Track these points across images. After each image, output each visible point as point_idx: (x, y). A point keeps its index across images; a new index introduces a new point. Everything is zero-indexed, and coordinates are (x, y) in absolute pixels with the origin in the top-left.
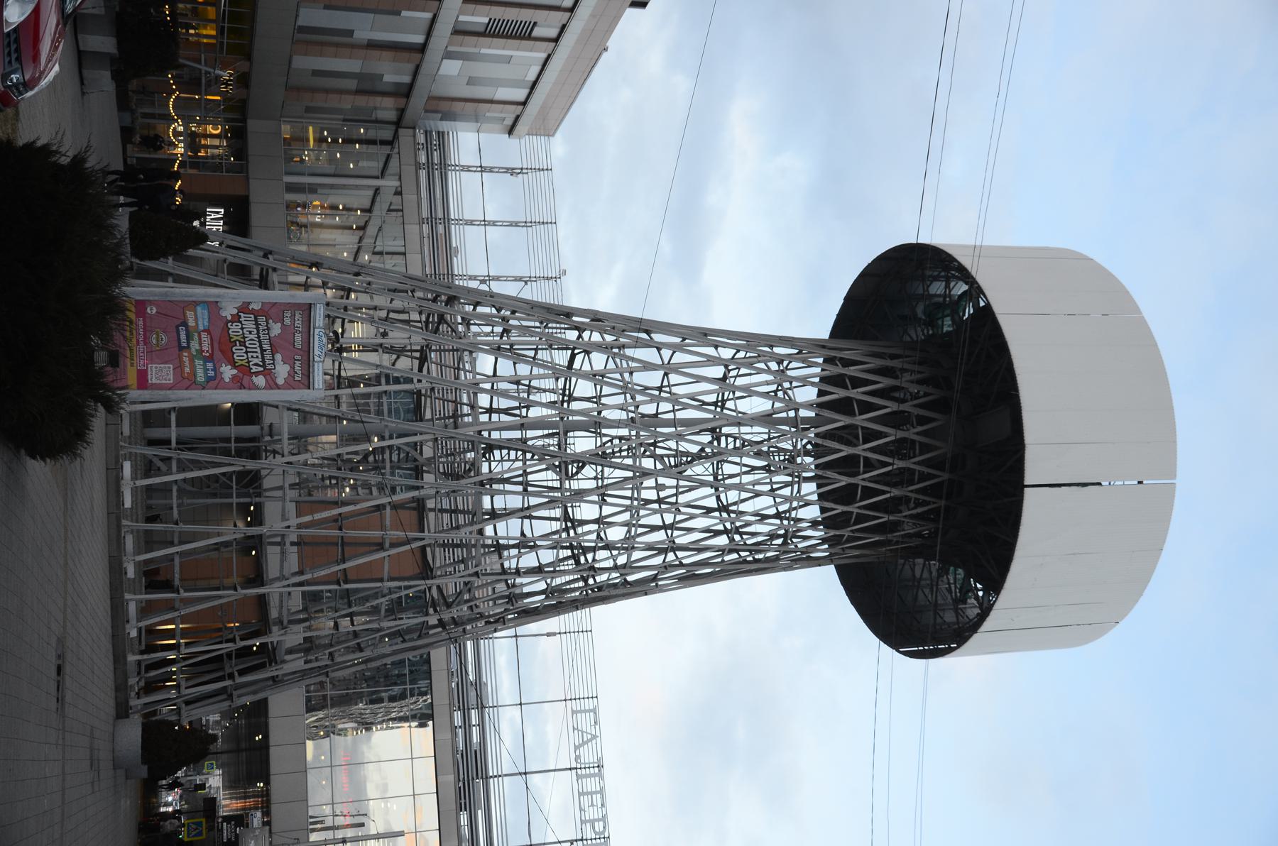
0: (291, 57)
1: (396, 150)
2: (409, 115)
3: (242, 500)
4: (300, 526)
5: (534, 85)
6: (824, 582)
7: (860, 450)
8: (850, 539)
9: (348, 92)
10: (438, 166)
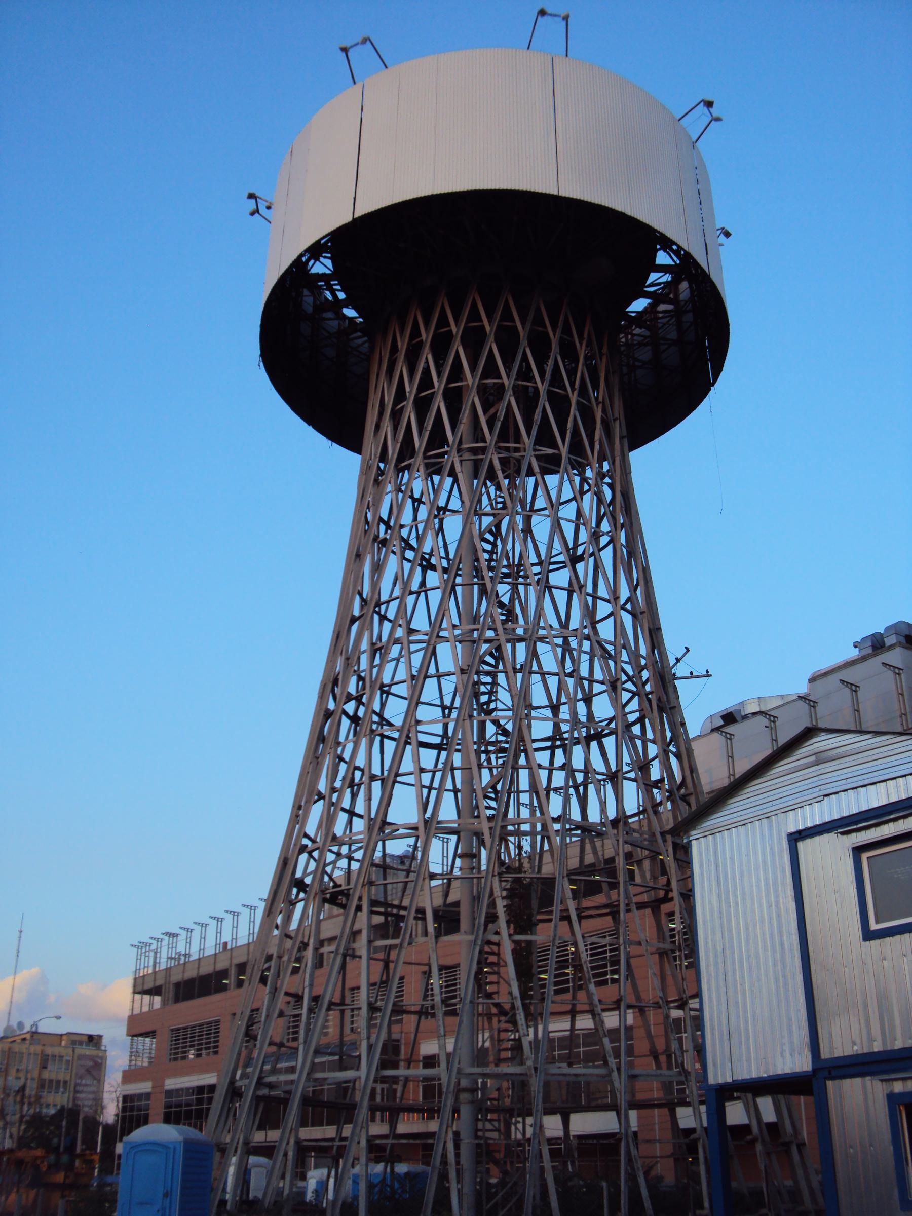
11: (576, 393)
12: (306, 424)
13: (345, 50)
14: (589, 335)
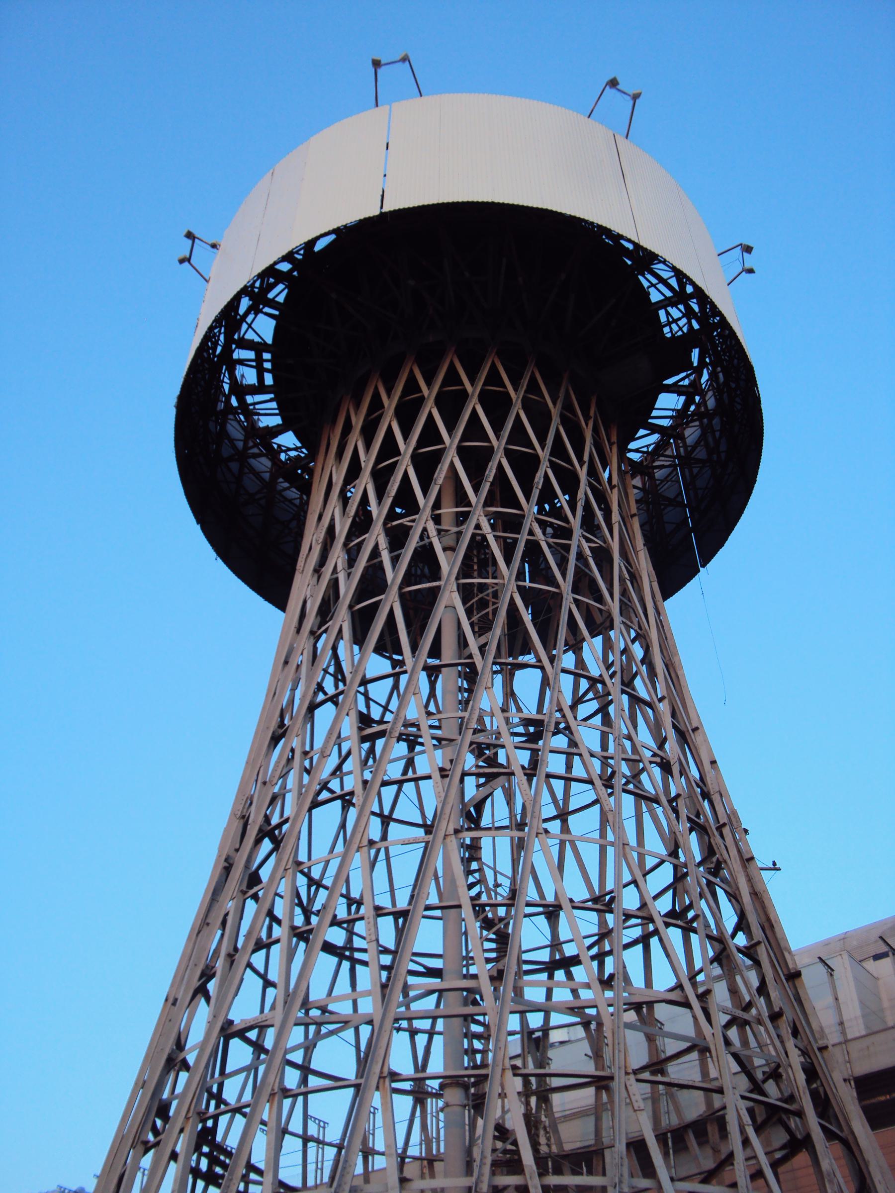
7: (406, 448)
12: (194, 521)
13: (377, 64)
14: (595, 414)
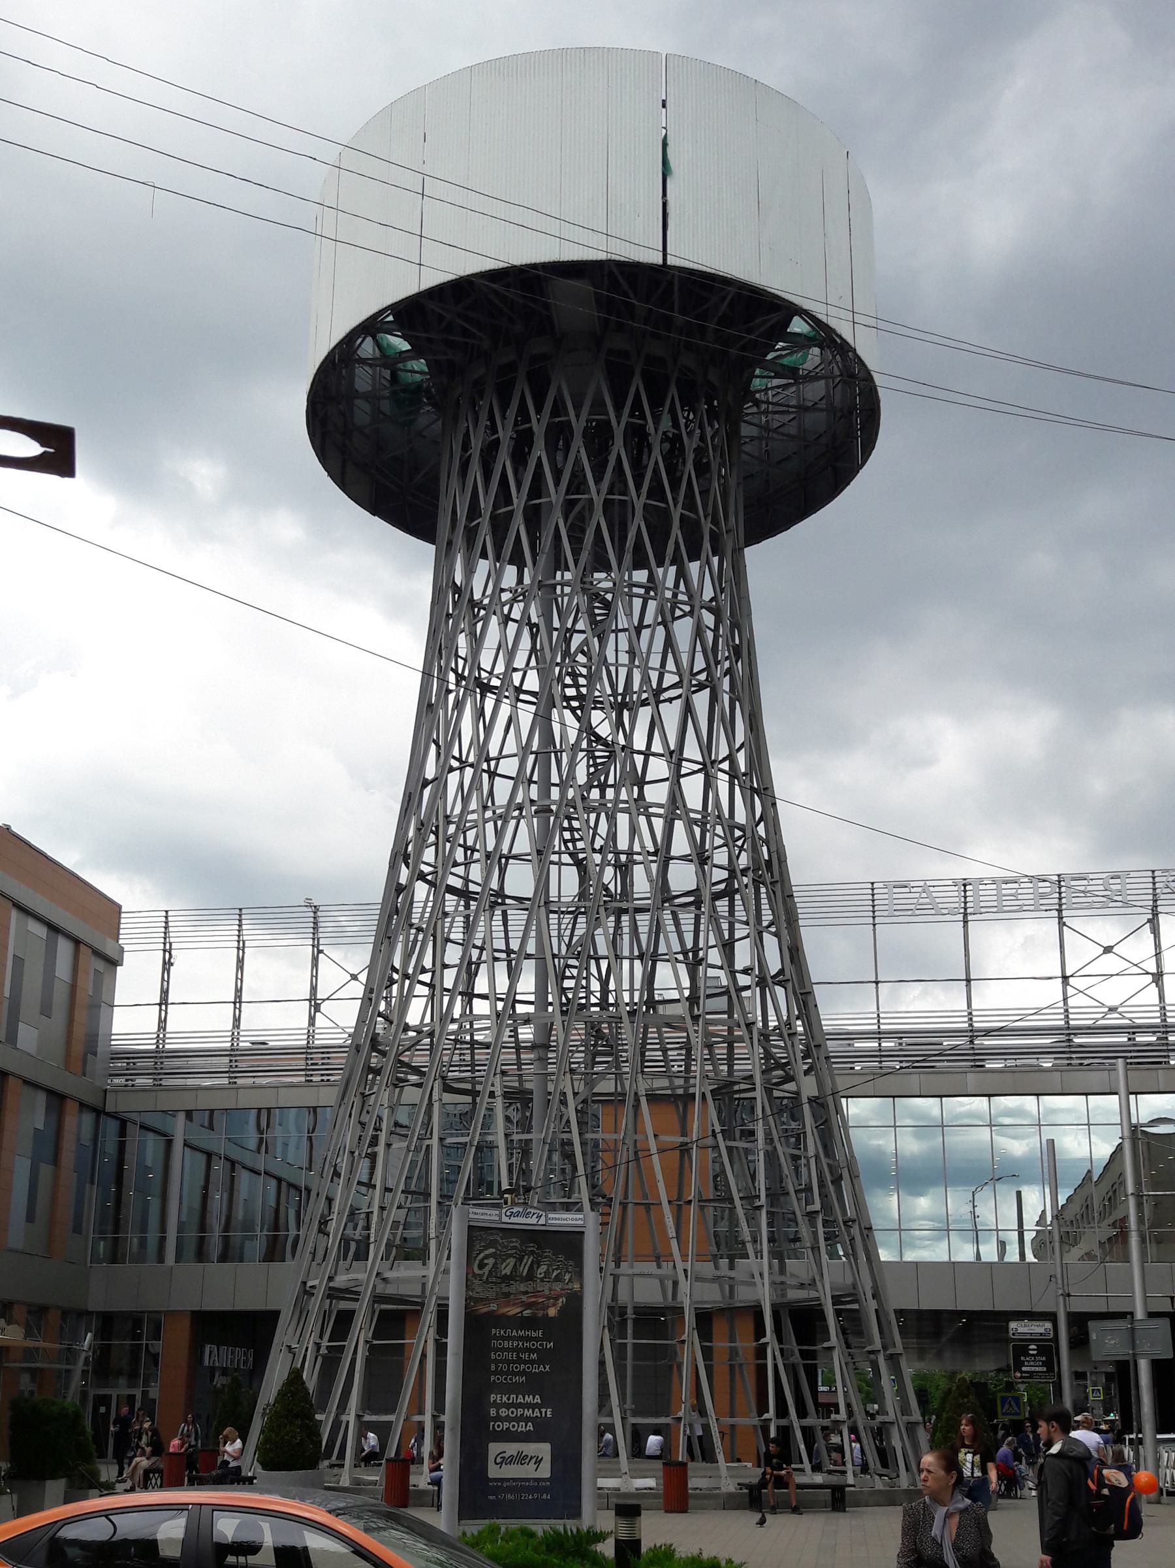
0: (11, 1250)
1: (135, 1116)
2: (93, 1099)
3: (630, 1331)
4: (684, 1257)
5: (53, 928)
6: (765, 561)
8: (715, 521)
9: (56, 1177)
10: (160, 1060)
11: (680, 505)
